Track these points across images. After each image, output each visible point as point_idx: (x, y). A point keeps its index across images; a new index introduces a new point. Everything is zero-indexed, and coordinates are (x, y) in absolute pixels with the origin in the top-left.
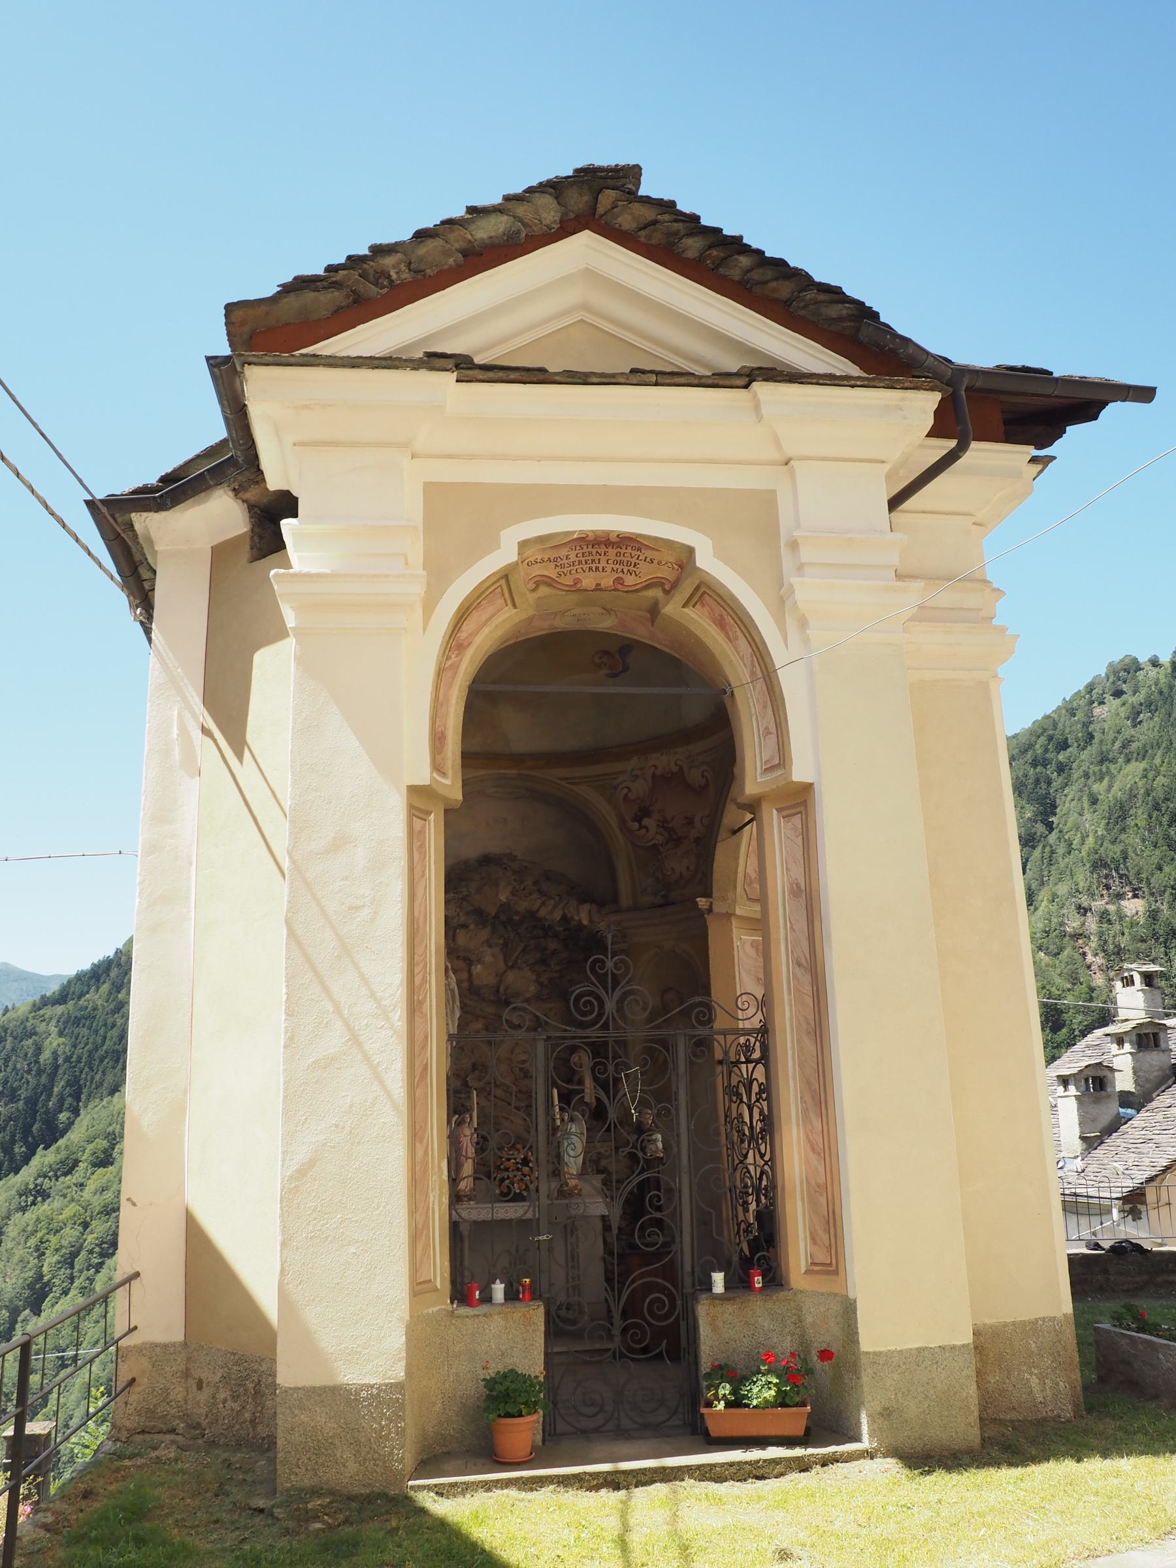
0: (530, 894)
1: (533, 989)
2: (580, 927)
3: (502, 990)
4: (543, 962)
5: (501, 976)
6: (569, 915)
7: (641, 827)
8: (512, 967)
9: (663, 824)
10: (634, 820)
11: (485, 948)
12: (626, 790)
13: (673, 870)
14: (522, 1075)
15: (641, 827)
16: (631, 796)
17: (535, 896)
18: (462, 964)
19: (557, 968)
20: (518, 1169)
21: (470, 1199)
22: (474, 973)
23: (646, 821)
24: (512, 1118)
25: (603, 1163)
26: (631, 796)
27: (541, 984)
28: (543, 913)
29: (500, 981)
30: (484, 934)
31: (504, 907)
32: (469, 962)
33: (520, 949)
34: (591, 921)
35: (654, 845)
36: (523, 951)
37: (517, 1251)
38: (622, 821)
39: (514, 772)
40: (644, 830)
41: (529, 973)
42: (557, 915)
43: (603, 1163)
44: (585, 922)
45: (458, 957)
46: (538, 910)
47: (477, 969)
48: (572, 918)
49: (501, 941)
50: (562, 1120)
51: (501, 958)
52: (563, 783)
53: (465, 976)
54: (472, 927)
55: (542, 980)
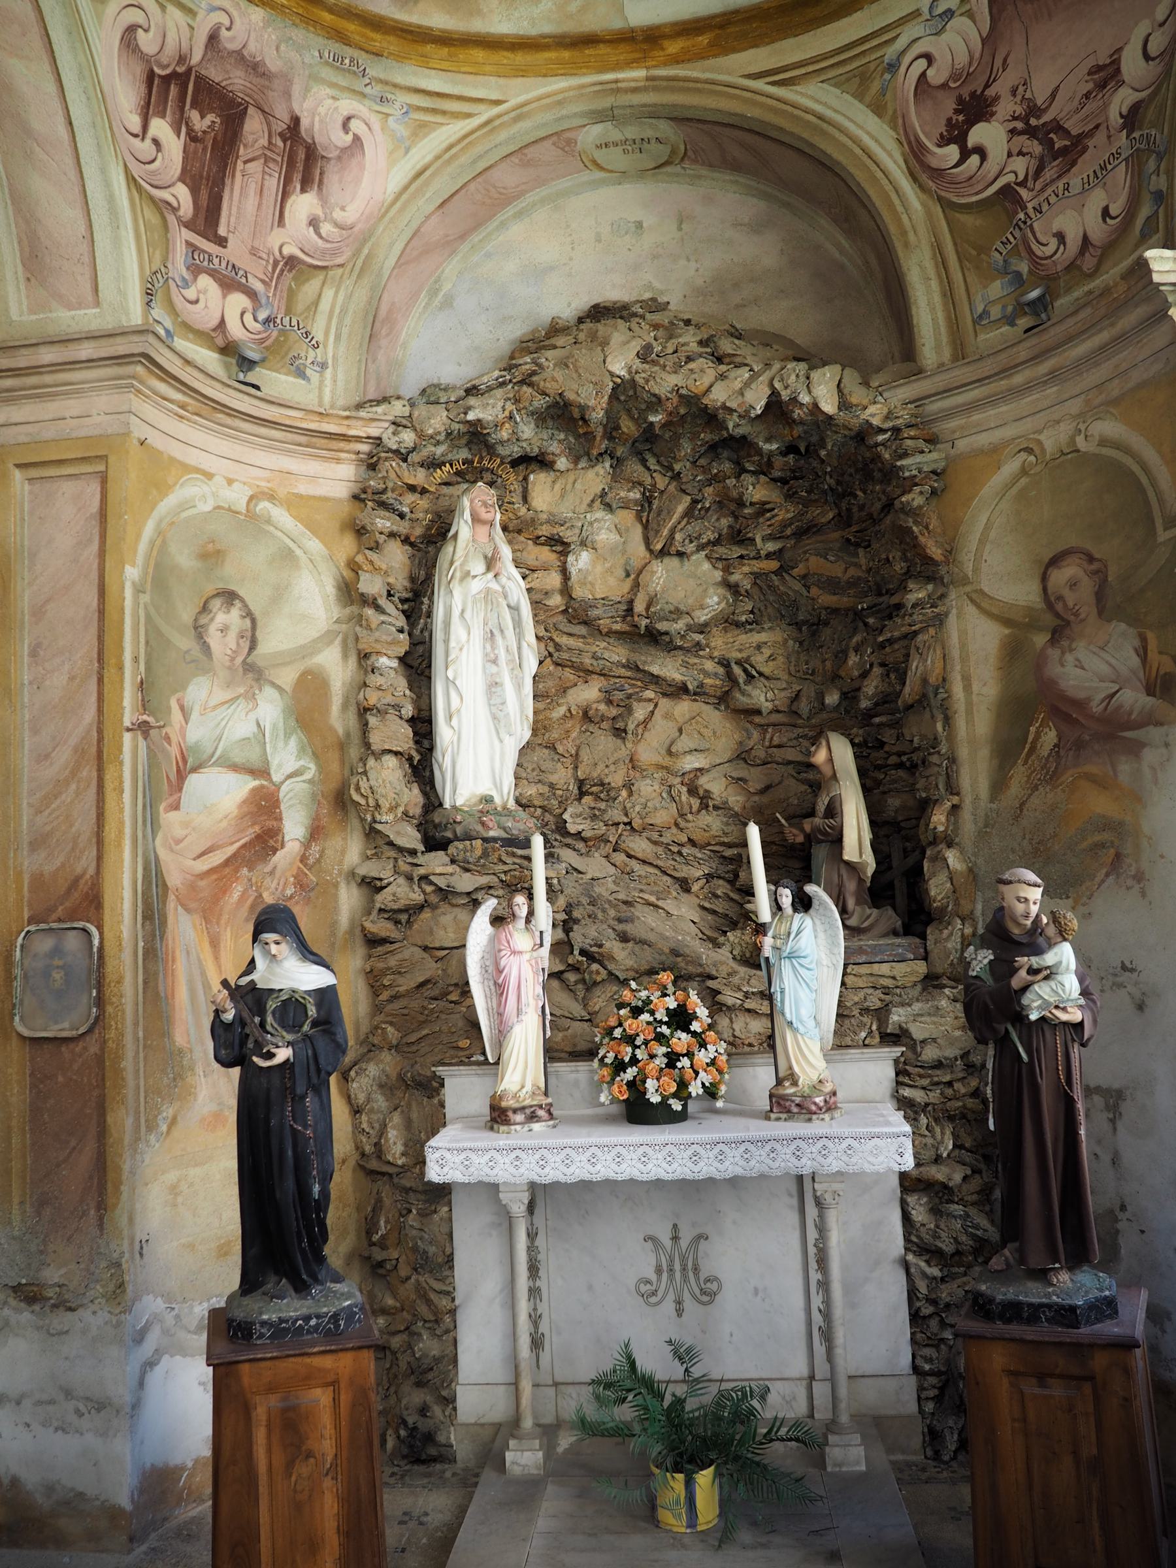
0: (689, 359)
1: (715, 602)
2: (820, 421)
3: (639, 607)
4: (738, 537)
5: (635, 577)
6: (785, 395)
7: (965, 154)
8: (663, 553)
9: (1031, 125)
10: (944, 141)
11: (600, 514)
12: (923, 62)
13: (1061, 237)
14: (695, 803)
15: (965, 154)
16: (936, 76)
17: (700, 363)
18: (546, 555)
19: (771, 546)
20: (660, 1038)
21: (532, 1118)
22: (573, 570)
23: (978, 134)
24: (669, 905)
25: (897, 1017)
26: (936, 76)
27: (734, 589)
28: (719, 395)
29: (636, 585)
30: (596, 478)
31: (625, 393)
32: (560, 546)
33: (680, 509)
34: (844, 405)
35: (1006, 191)
36: (688, 514)
37: (675, 1239)
38: (915, 153)
39: (640, 73)
40: (975, 159)
41: (706, 566)
42: (757, 399)
43: (897, 1017)
44: (829, 406)
45: (536, 540)
46: (709, 390)
47: (580, 561)
48: (794, 400)
49: (635, 495)
50: (777, 907)
51: (638, 531)
52: (759, 85)
53: (554, 580)
54: (562, 463)
55: (735, 578)
